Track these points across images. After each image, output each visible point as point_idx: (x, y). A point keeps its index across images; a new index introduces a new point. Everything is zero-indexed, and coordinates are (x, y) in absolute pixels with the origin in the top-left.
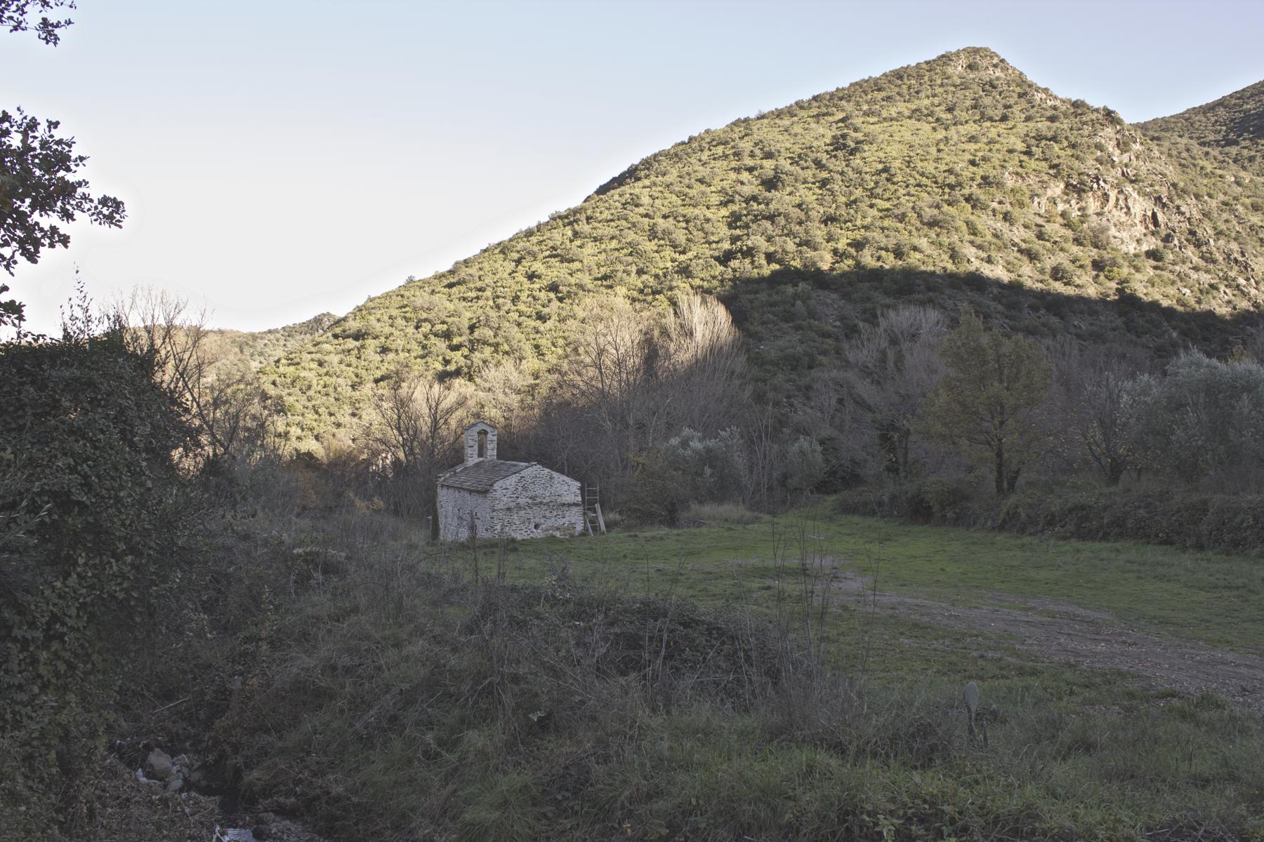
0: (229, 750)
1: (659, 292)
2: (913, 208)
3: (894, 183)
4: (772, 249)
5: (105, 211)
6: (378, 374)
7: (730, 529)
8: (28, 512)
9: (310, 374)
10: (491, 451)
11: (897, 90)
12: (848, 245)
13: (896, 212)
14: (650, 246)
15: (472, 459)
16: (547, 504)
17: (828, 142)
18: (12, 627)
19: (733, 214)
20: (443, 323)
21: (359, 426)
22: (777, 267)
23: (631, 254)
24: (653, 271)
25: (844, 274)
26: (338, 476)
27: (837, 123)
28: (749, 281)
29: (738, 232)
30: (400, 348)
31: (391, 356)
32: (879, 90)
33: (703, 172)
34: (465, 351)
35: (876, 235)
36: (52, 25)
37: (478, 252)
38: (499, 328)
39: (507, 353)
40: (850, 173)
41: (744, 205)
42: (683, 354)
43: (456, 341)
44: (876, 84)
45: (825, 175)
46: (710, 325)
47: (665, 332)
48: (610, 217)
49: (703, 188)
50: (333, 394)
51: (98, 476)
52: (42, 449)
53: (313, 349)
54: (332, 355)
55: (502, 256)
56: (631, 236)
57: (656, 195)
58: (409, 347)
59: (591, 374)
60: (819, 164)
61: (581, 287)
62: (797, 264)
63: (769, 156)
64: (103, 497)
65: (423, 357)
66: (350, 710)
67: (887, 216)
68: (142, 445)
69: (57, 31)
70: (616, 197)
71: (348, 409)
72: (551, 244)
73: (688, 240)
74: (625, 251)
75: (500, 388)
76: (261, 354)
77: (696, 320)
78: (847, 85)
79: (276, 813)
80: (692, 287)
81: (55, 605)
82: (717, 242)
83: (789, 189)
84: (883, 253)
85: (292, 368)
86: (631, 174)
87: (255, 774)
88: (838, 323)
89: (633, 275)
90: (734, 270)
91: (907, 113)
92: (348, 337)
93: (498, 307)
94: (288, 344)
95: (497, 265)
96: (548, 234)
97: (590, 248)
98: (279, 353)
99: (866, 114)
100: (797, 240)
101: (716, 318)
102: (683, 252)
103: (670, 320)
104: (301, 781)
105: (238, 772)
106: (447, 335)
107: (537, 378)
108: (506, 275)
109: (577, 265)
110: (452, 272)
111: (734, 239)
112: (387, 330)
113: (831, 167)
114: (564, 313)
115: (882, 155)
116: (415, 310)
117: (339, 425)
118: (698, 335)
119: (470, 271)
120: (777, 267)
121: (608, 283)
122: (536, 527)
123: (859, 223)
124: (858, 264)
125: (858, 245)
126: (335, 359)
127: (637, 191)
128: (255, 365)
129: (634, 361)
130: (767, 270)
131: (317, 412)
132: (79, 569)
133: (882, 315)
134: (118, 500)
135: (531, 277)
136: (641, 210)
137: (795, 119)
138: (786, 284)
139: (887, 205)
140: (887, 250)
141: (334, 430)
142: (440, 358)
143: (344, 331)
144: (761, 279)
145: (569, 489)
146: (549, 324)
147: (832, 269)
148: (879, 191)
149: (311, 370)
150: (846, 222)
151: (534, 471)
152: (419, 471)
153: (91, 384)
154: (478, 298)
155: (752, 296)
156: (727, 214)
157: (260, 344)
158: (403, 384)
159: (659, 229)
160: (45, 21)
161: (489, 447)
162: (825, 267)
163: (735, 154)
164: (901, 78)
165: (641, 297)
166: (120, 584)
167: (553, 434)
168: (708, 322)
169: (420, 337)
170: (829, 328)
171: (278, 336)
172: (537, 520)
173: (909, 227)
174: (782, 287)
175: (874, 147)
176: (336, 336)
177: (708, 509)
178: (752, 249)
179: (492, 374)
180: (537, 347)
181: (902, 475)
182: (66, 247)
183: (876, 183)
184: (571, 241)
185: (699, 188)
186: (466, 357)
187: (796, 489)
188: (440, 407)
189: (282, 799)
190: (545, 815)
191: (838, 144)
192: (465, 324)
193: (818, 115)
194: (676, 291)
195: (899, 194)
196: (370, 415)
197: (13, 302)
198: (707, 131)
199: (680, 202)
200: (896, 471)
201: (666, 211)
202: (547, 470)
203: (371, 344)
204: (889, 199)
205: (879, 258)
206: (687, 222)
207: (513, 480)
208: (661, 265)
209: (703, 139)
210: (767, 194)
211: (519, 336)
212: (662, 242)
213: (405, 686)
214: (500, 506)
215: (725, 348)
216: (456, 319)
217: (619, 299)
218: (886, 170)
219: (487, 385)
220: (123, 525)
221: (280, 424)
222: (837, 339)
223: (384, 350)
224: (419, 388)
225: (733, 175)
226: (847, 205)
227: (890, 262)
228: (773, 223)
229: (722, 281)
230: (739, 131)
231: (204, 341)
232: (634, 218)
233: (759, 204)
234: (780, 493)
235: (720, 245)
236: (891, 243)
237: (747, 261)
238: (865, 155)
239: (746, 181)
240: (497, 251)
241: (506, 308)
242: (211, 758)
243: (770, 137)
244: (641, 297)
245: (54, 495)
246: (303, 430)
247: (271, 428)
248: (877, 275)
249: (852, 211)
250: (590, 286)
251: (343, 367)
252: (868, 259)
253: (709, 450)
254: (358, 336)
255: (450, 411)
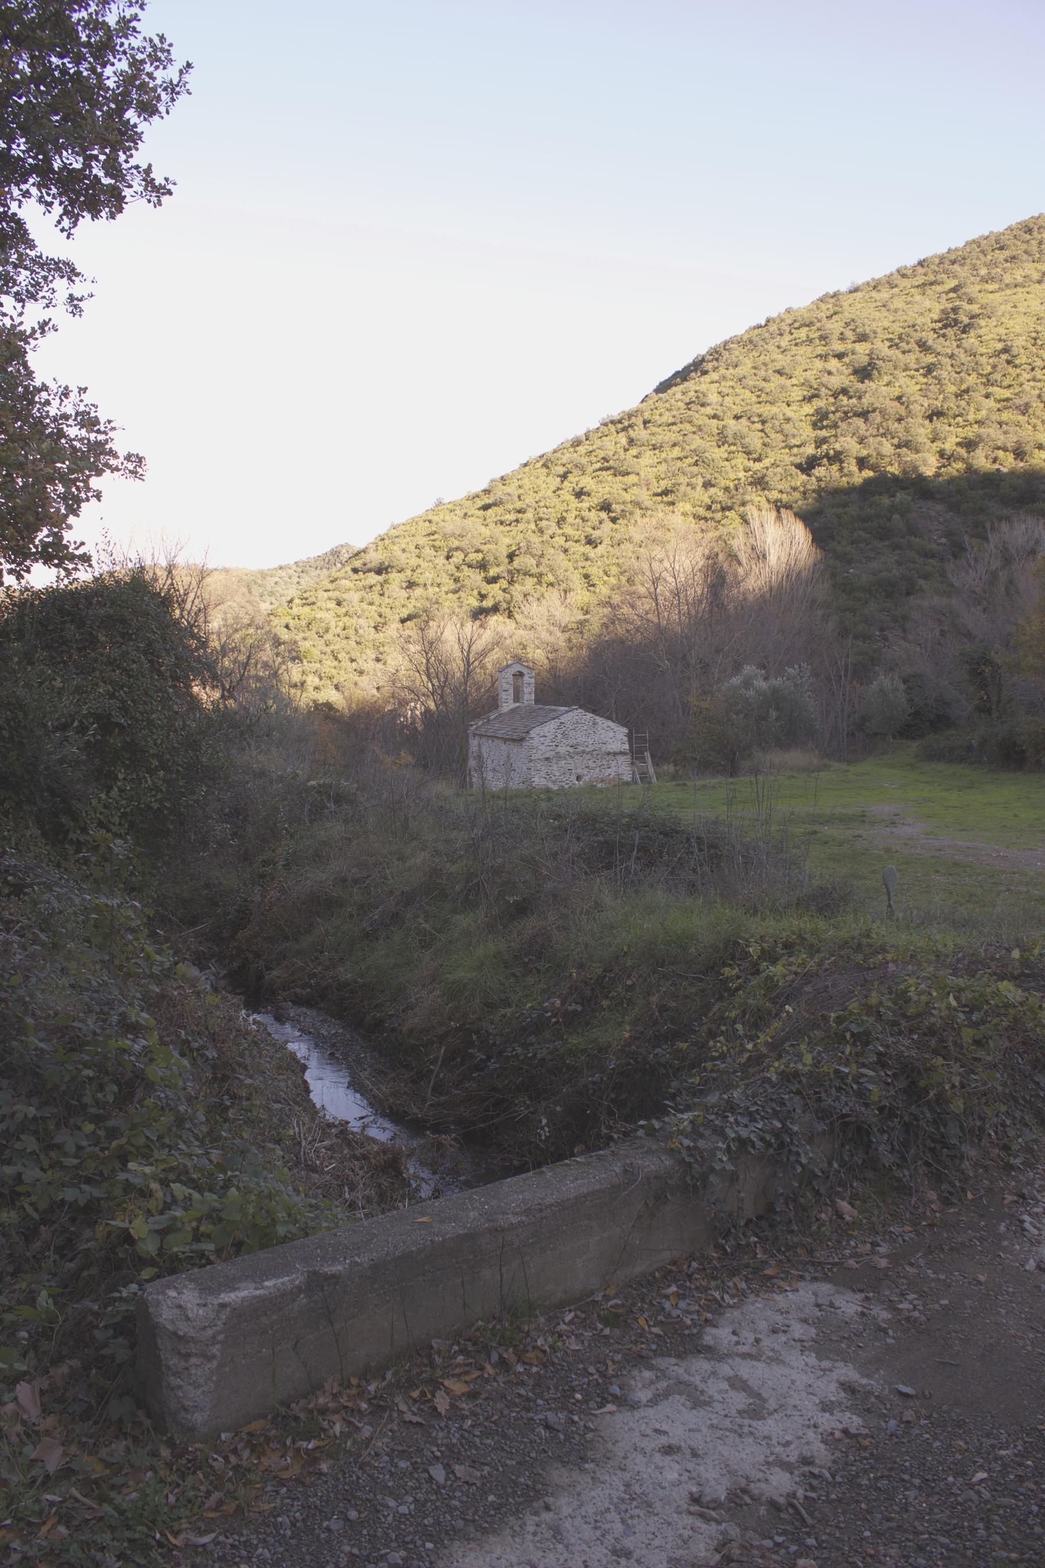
0: (250, 956)
1: (730, 509)
2: (1039, 396)
3: (1016, 366)
4: (864, 453)
5: (131, 466)
6: (405, 612)
7: (793, 777)
8: (77, 733)
9: (327, 614)
10: (529, 696)
11: (1024, 247)
12: (958, 444)
13: (1018, 402)
14: (720, 453)
15: (507, 704)
16: (591, 753)
17: (936, 317)
18: (68, 831)
19: (818, 411)
20: (478, 551)
21: (384, 672)
22: (871, 474)
23: (696, 464)
24: (723, 483)
25: (952, 480)
26: (359, 729)
27: (947, 293)
28: (837, 492)
29: (824, 433)
30: (429, 582)
31: (418, 591)
32: (1001, 248)
33: (783, 361)
34: (504, 583)
35: (992, 432)
36: (77, 299)
37: (517, 467)
38: (542, 556)
39: (552, 584)
40: (962, 355)
41: (832, 400)
42: (754, 580)
43: (493, 572)
44: (997, 242)
45: (930, 359)
46: (787, 545)
47: (733, 557)
48: (671, 420)
49: (782, 380)
50: (353, 638)
51: (133, 701)
52: (86, 679)
53: (330, 586)
54: (352, 593)
55: (544, 470)
56: (697, 442)
57: (726, 391)
58: (439, 580)
59: (647, 607)
60: (923, 346)
61: (637, 504)
62: (894, 469)
63: (862, 338)
64: (137, 720)
65: (455, 592)
66: (358, 915)
67: (1006, 408)
68: (168, 674)
69: (81, 304)
70: (679, 396)
71: (371, 654)
72: (602, 454)
73: (764, 445)
74: (690, 460)
75: (543, 625)
76: (272, 594)
77: (769, 540)
78: (961, 244)
79: (293, 1002)
80: (768, 501)
81: (101, 813)
82: (799, 446)
83: (886, 379)
84: (1000, 454)
85: (307, 609)
86: (697, 367)
87: (275, 973)
88: (944, 540)
89: (699, 488)
90: (819, 480)
91: (1036, 276)
92: (370, 571)
93: (541, 531)
94: (302, 581)
95: (540, 482)
96: (598, 443)
97: (648, 458)
98: (292, 592)
99: (985, 280)
100: (896, 441)
101: (793, 537)
102: (758, 460)
103: (739, 543)
104: (315, 975)
105: (260, 977)
106: (483, 566)
107: (587, 612)
108: (549, 493)
109: (632, 479)
110: (487, 492)
111: (820, 442)
112: (414, 562)
113: (939, 349)
114: (618, 536)
115: (1002, 331)
116: (445, 537)
117: (361, 673)
118: (772, 559)
119: (508, 489)
120: (871, 474)
121: (669, 498)
122: (578, 778)
123: (971, 417)
124: (969, 469)
125: (970, 445)
126: (355, 597)
127: (703, 387)
128: (265, 607)
129: (697, 590)
130: (859, 477)
131: (336, 659)
132: (119, 784)
133: (992, 529)
134: (150, 722)
135: (579, 494)
136: (709, 410)
137: (896, 290)
138: (880, 494)
139: (1007, 393)
140: (1005, 450)
141: (357, 678)
142: (475, 592)
143: (365, 565)
144: (852, 490)
145: (613, 736)
146: (601, 549)
147: (937, 475)
148: (997, 376)
149: (328, 610)
150: (955, 417)
151: (575, 717)
152: (451, 722)
153: (123, 621)
154: (517, 521)
155: (840, 510)
156: (811, 411)
157: (270, 582)
158: (431, 623)
159: (729, 433)
160: (71, 298)
161: (526, 690)
162: (929, 472)
163: (822, 338)
164: (1029, 231)
165: (709, 515)
166: (155, 796)
167: (610, 675)
168: (780, 544)
169: (452, 568)
170: (934, 546)
171: (291, 572)
172: (579, 771)
173: (1033, 421)
174: (877, 498)
175: (993, 322)
176: (355, 571)
177: (776, 757)
178: (841, 453)
179: (535, 610)
180: (586, 576)
181: (995, 715)
182: (99, 500)
183: (994, 367)
184: (626, 450)
185: (778, 380)
186: (504, 590)
187: (876, 734)
188: (473, 648)
189: (298, 990)
190: (514, 975)
191: (949, 321)
192: (504, 552)
193: (924, 285)
194: (748, 507)
195: (1022, 379)
196: (396, 660)
197: (85, 554)
198: (788, 311)
199: (754, 399)
200: (989, 712)
201: (737, 410)
202: (590, 715)
203: (394, 576)
204: (1009, 386)
205: (995, 460)
206: (763, 422)
207: (551, 727)
208: (732, 476)
209: (782, 320)
210: (860, 386)
211: (566, 564)
212: (733, 448)
213: (407, 889)
214: (537, 756)
215: (804, 574)
216: (492, 547)
217: (679, 519)
218: (1006, 350)
219: (528, 622)
220: (155, 744)
221: (295, 673)
222: (942, 560)
223: (411, 585)
224: (449, 626)
225: (819, 364)
226: (957, 396)
227: (1008, 463)
228: (866, 420)
229: (804, 493)
230: (828, 308)
231: (208, 580)
232: (700, 419)
233: (850, 397)
234: (862, 738)
235: (802, 450)
236: (1010, 441)
237: (835, 468)
238: (981, 332)
239: (834, 370)
240: (539, 465)
241: (550, 532)
242: (236, 964)
243: (864, 314)
244: (709, 515)
245: (98, 717)
246: (321, 679)
247: (286, 677)
248: (991, 481)
249: (963, 403)
250: (648, 503)
251: (364, 605)
252: (981, 460)
253: (775, 691)
254: (381, 570)
255: (484, 653)
